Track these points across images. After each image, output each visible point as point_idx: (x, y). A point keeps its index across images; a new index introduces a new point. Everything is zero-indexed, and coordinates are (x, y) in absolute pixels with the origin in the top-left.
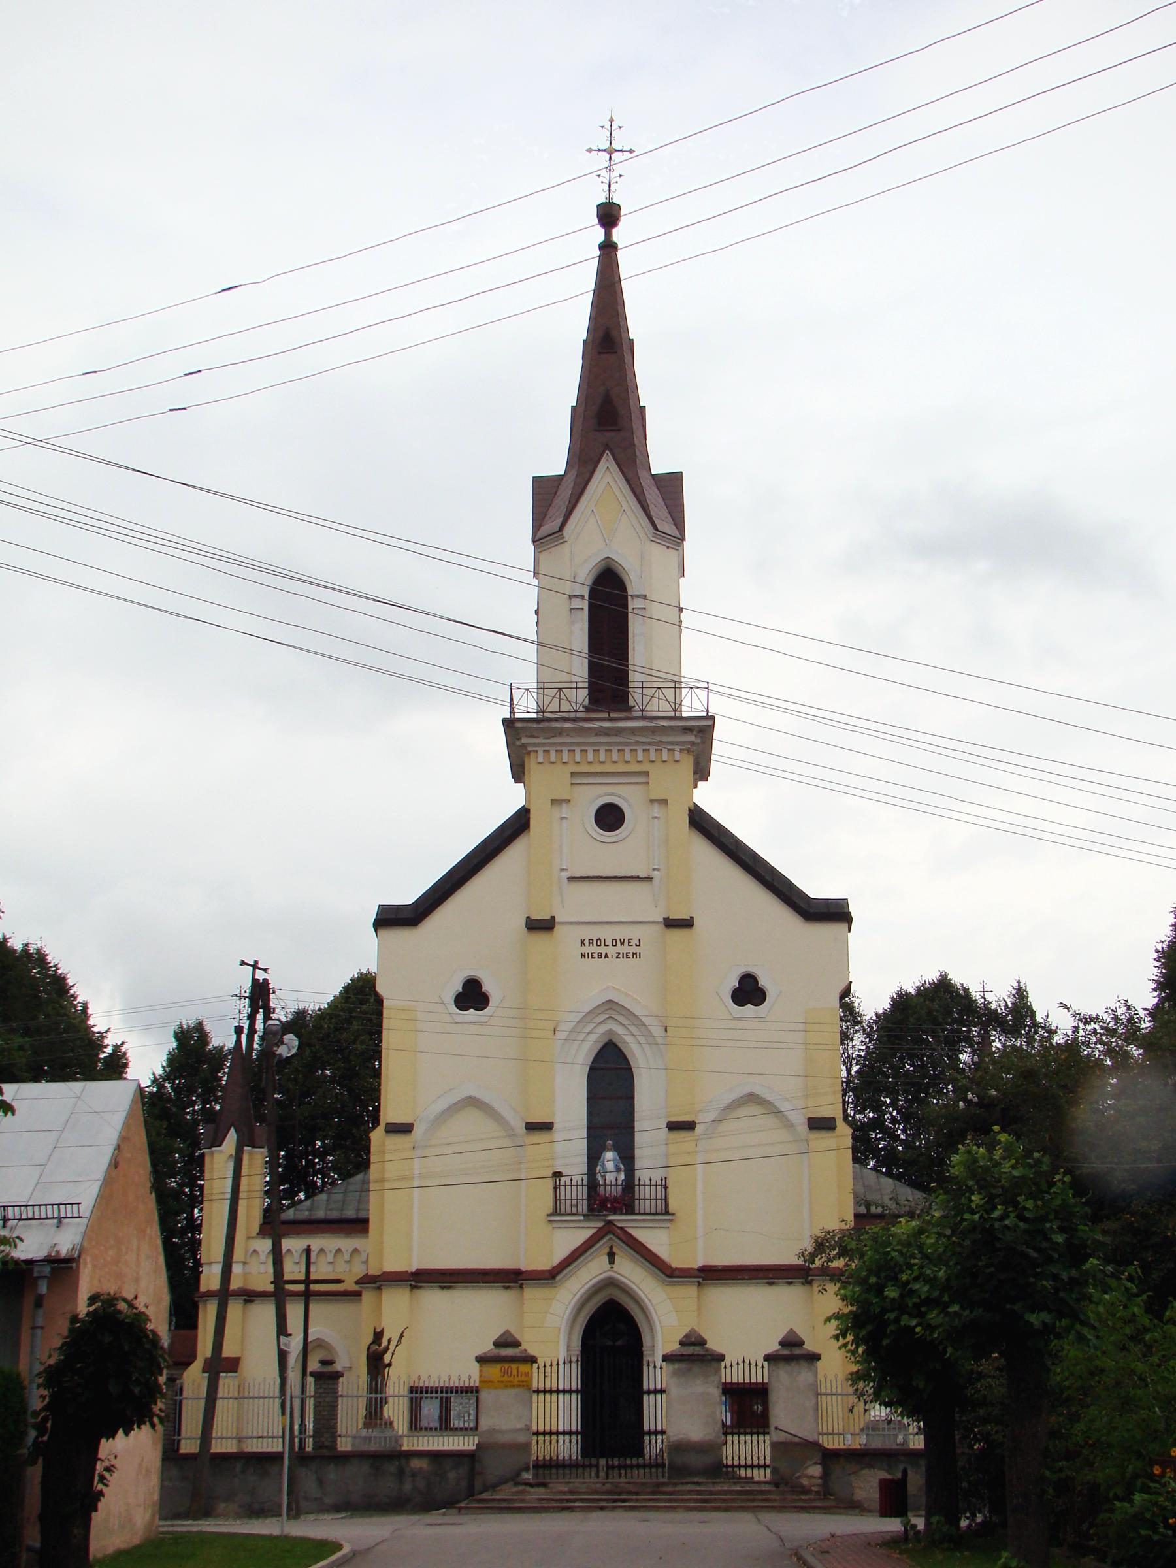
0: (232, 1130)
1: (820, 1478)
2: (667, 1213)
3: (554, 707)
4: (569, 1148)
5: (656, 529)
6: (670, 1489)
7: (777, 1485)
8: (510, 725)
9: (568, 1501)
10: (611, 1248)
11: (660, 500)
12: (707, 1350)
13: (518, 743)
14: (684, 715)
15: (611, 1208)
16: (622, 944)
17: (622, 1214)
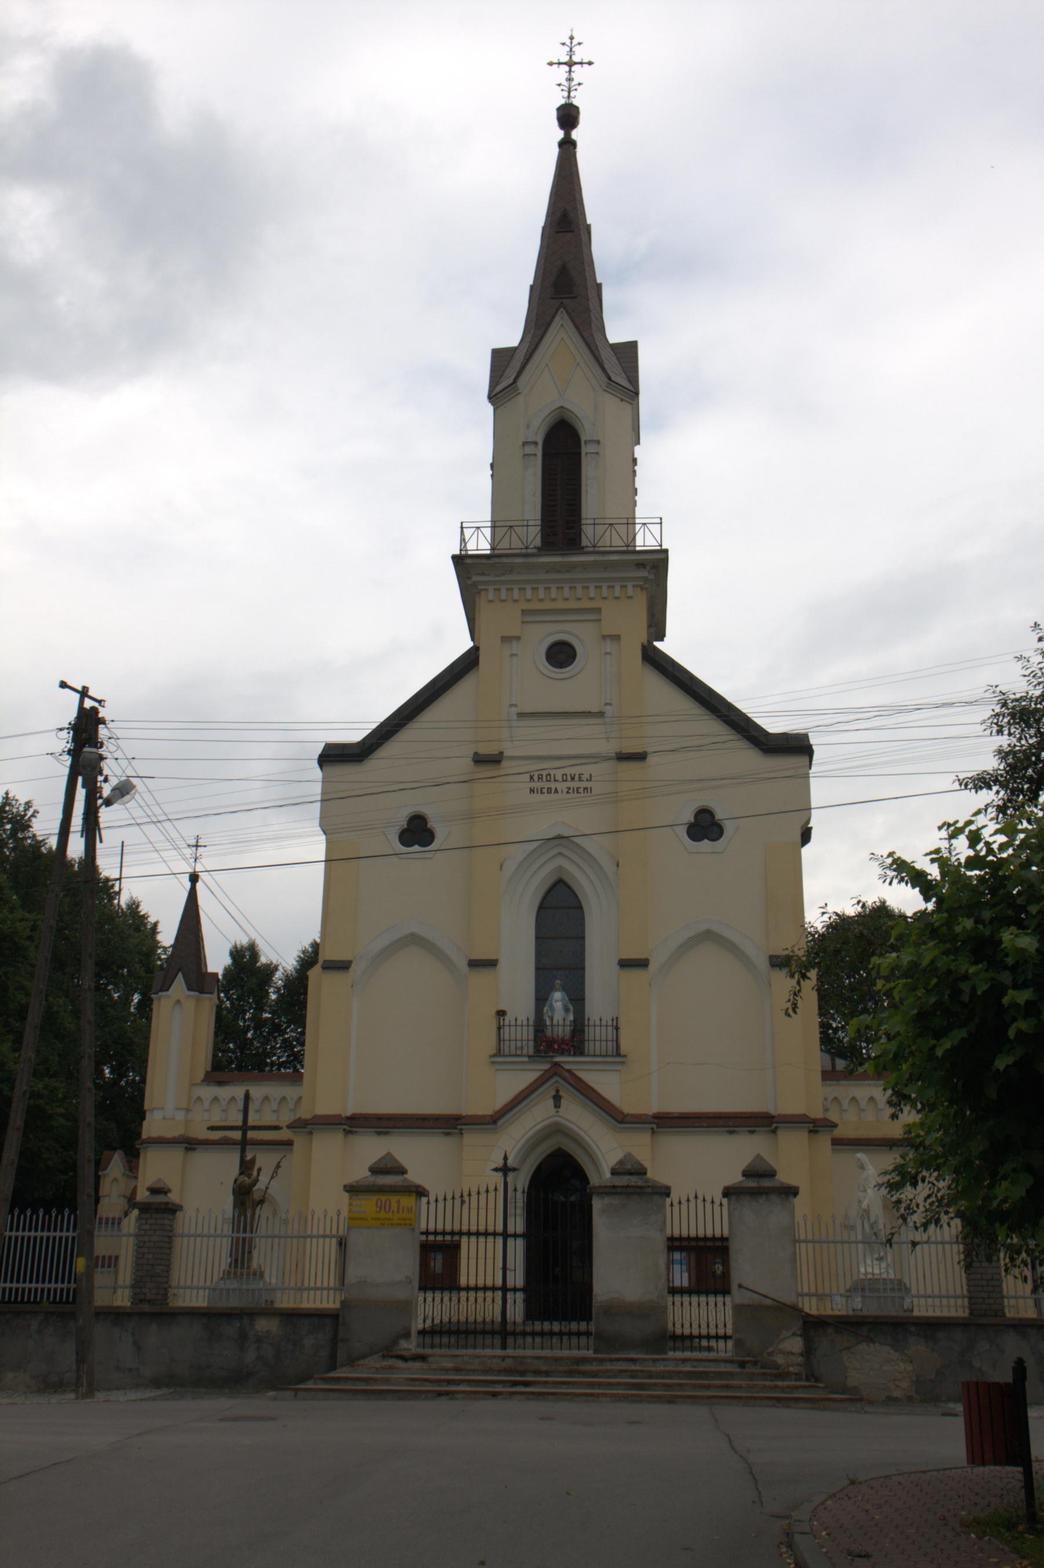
0: (180, 975)
1: (801, 1354)
2: (618, 1055)
3: (504, 544)
4: (515, 985)
5: (610, 379)
6: (594, 1367)
7: (742, 1364)
8: (462, 562)
9: (449, 1382)
10: (557, 1091)
11: (614, 359)
12: (647, 1181)
13: (469, 582)
14: (638, 549)
15: (558, 1048)
16: (573, 779)
17: (569, 1055)
